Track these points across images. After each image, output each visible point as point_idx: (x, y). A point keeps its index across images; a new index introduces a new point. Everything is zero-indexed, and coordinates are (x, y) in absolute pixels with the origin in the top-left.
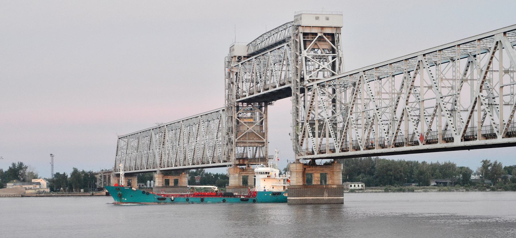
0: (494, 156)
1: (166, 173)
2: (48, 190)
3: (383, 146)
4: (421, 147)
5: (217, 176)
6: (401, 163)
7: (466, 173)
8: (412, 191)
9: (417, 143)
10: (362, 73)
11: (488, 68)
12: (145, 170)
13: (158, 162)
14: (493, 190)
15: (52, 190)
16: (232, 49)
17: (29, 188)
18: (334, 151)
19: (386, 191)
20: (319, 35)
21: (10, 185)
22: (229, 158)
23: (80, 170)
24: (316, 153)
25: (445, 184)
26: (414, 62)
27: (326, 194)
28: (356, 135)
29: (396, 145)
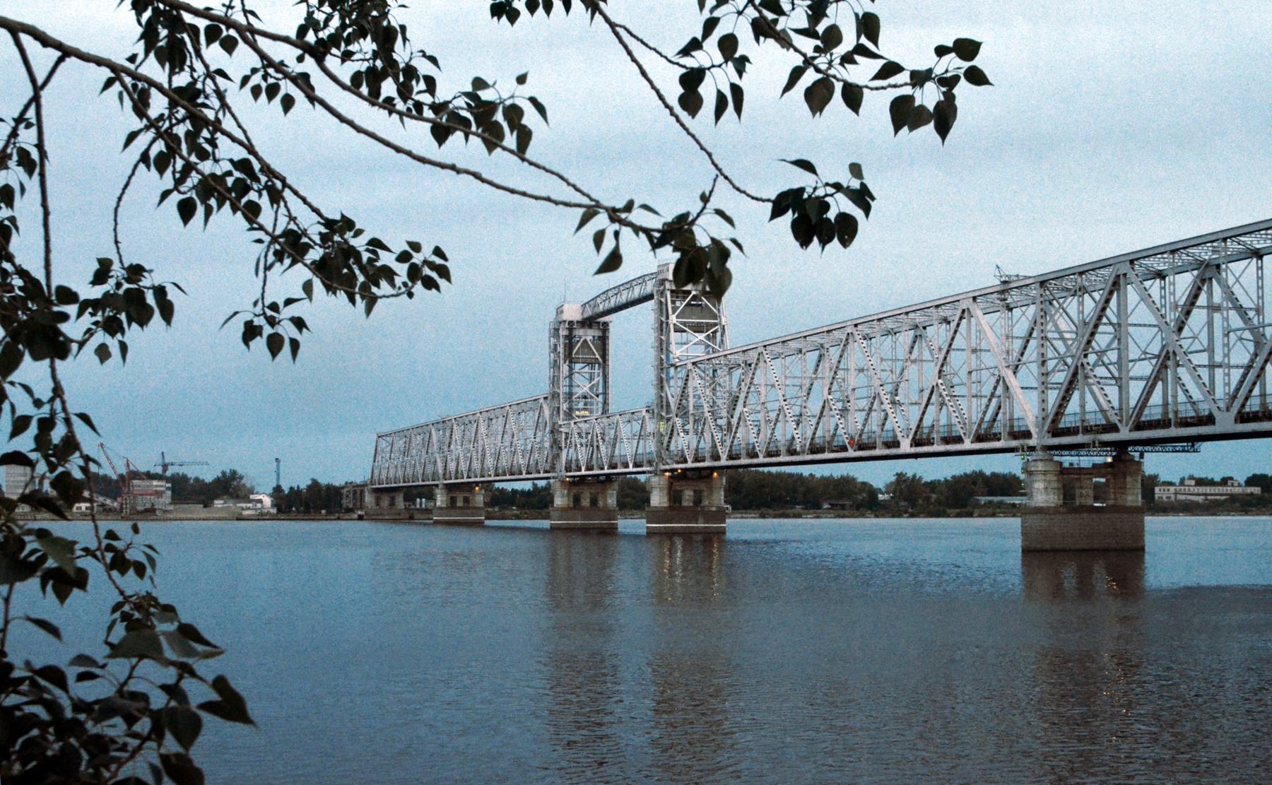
0: (910, 468)
1: (450, 488)
2: (274, 511)
3: (792, 452)
4: (851, 453)
5: (514, 492)
6: (779, 475)
7: (872, 492)
8: (799, 516)
9: (844, 449)
10: (762, 349)
11: (950, 345)
12: (421, 483)
13: (441, 471)
14: (912, 516)
15: (279, 511)
16: (559, 311)
17: (248, 509)
18: (626, 466)
19: (763, 516)
20: (694, 293)
21: (218, 503)
22: (553, 468)
23: (323, 481)
24: (689, 460)
25: (843, 507)
26: (754, 354)
27: (701, 519)
28: (746, 435)
29: (813, 452)
